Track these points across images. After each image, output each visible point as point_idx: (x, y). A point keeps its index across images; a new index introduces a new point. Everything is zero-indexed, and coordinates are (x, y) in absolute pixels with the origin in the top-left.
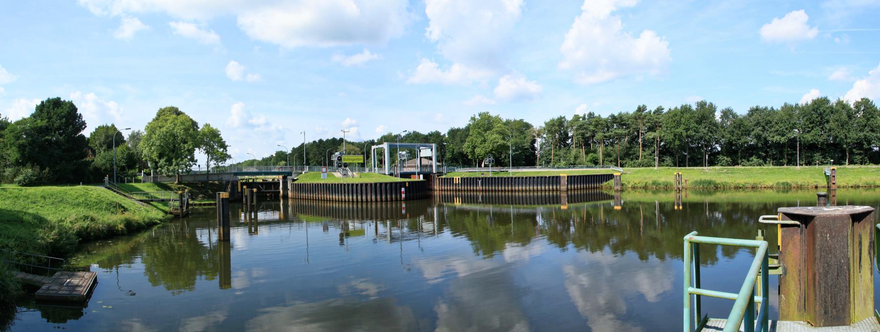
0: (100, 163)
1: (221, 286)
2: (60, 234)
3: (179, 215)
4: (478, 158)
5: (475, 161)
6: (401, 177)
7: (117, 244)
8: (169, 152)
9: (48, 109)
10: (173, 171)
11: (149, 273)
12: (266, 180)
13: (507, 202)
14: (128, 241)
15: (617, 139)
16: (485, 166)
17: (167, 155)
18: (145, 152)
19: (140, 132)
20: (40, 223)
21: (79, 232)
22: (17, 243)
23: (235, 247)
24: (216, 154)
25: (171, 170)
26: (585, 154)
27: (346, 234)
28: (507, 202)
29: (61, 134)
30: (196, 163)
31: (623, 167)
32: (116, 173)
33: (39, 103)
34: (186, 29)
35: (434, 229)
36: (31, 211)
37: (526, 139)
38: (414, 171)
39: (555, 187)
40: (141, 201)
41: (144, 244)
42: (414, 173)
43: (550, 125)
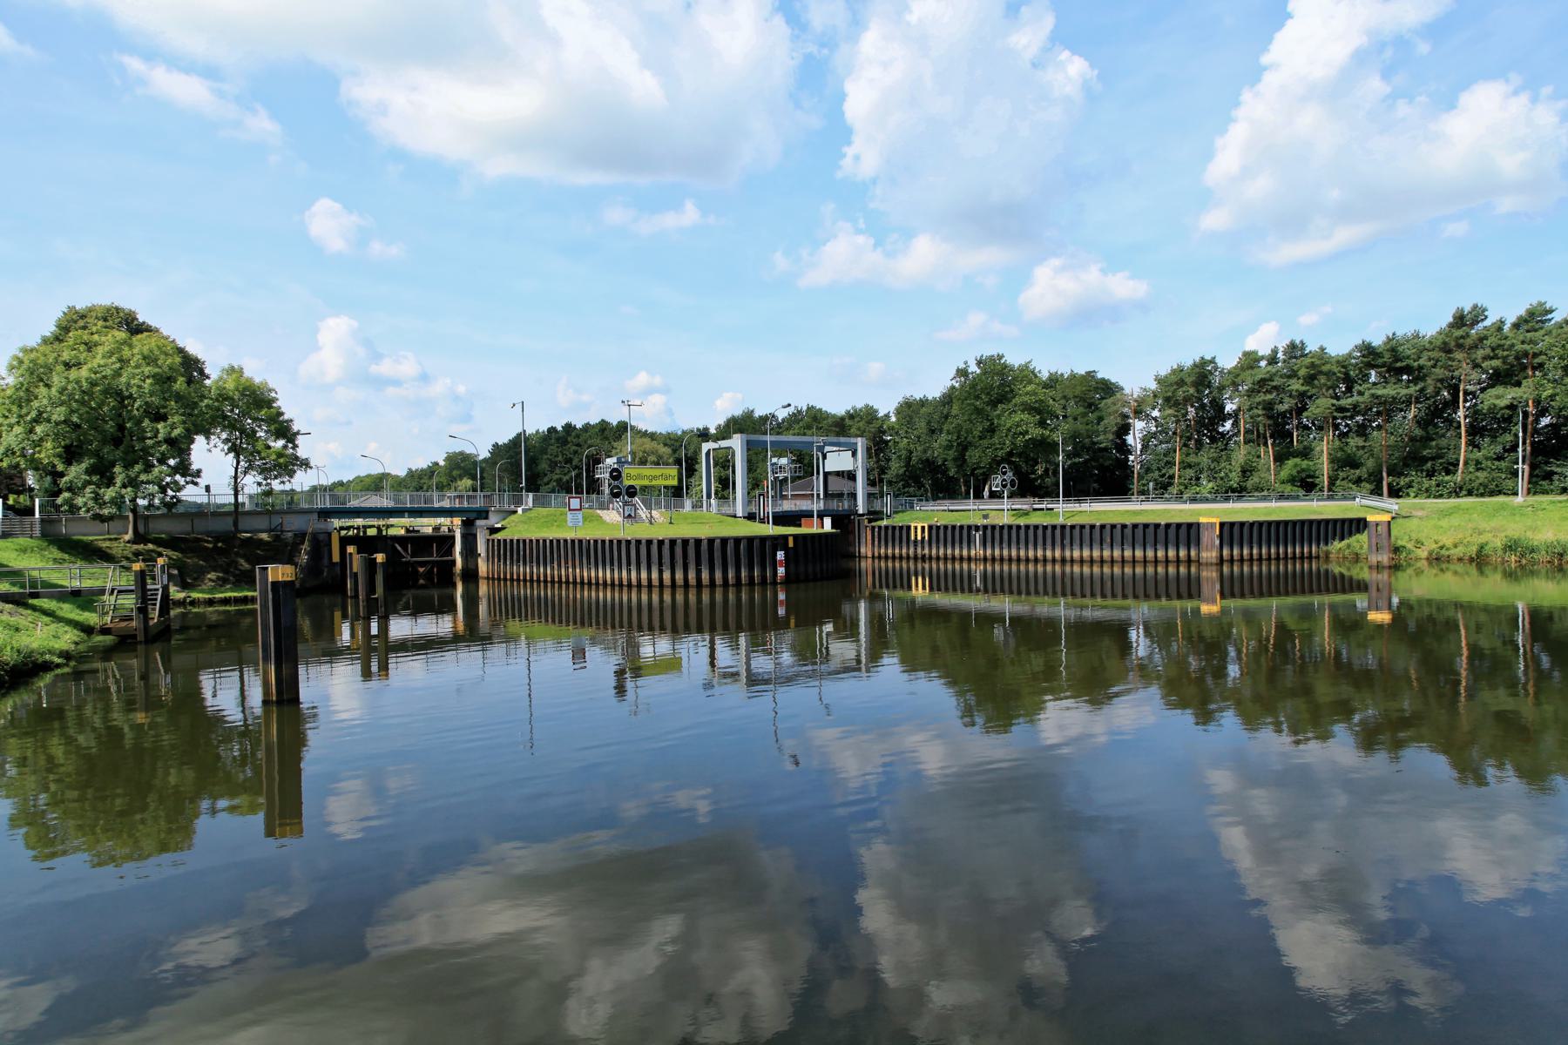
3: (134, 637)
4: (972, 474)
6: (776, 523)
8: (104, 442)
10: (118, 502)
12: (414, 531)
13: (1050, 590)
15: (1379, 413)
16: (993, 495)
24: (263, 455)
25: (107, 498)
26: (1276, 460)
28: (1050, 590)
30: (198, 480)
31: (1401, 497)
35: (859, 655)
37: (1102, 423)
38: (809, 508)
39: (1183, 553)
42: (809, 515)
43: (1171, 385)
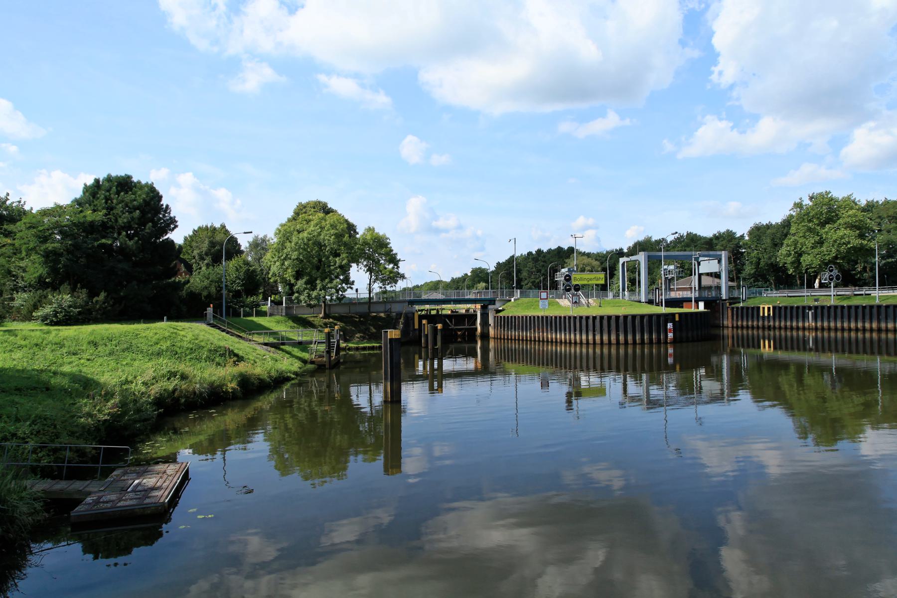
0: (200, 286)
1: (386, 471)
2: (123, 404)
3: (325, 365)
4: (806, 272)
5: (802, 278)
7: (226, 414)
8: (312, 269)
9: (108, 194)
10: (317, 298)
11: (275, 456)
14: (243, 408)
17: (309, 274)
18: (274, 269)
19: (267, 239)
20: (84, 389)
21: (159, 398)
22: (36, 427)
23: (408, 411)
24: (383, 272)
25: (313, 296)
27: (575, 393)
29: (130, 237)
30: (353, 286)
32: (227, 303)
33: (90, 181)
34: (343, 87)
36: (66, 369)
40: (266, 344)
41: (268, 411)
42: (689, 300)
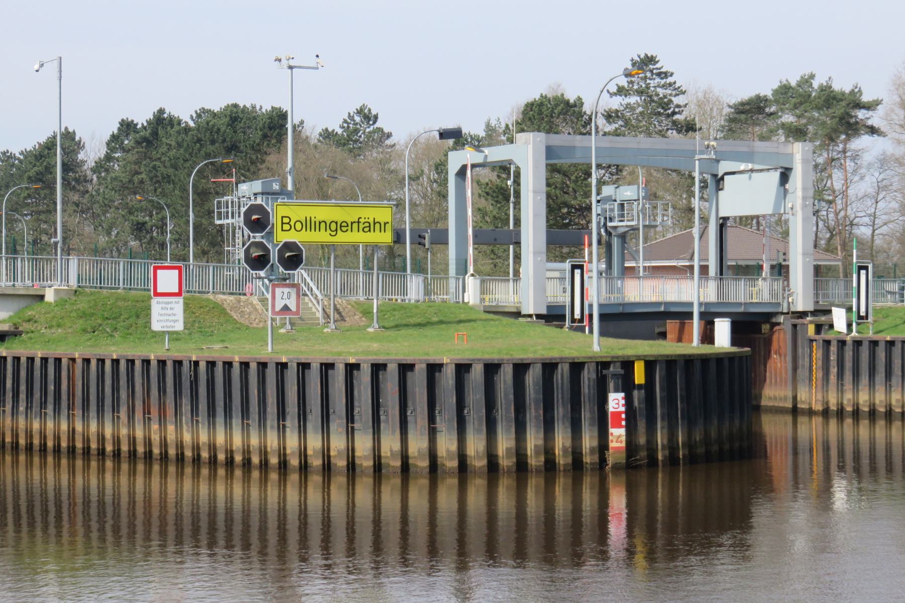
42: (682, 315)
